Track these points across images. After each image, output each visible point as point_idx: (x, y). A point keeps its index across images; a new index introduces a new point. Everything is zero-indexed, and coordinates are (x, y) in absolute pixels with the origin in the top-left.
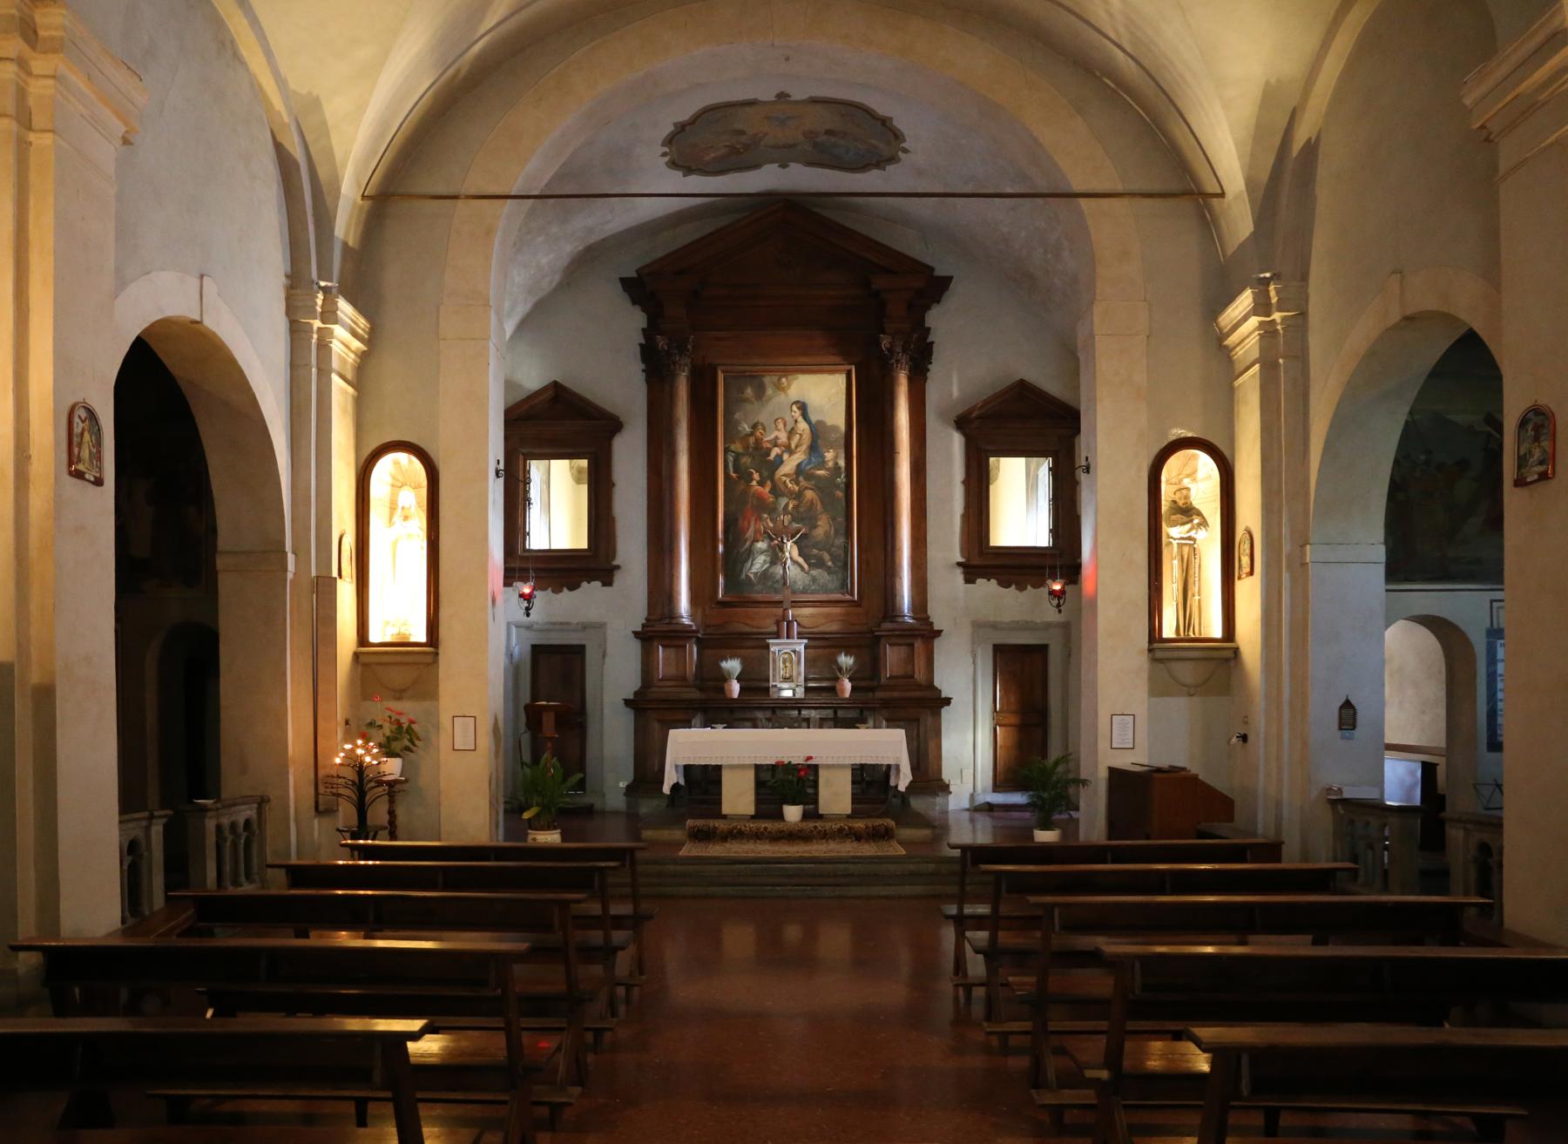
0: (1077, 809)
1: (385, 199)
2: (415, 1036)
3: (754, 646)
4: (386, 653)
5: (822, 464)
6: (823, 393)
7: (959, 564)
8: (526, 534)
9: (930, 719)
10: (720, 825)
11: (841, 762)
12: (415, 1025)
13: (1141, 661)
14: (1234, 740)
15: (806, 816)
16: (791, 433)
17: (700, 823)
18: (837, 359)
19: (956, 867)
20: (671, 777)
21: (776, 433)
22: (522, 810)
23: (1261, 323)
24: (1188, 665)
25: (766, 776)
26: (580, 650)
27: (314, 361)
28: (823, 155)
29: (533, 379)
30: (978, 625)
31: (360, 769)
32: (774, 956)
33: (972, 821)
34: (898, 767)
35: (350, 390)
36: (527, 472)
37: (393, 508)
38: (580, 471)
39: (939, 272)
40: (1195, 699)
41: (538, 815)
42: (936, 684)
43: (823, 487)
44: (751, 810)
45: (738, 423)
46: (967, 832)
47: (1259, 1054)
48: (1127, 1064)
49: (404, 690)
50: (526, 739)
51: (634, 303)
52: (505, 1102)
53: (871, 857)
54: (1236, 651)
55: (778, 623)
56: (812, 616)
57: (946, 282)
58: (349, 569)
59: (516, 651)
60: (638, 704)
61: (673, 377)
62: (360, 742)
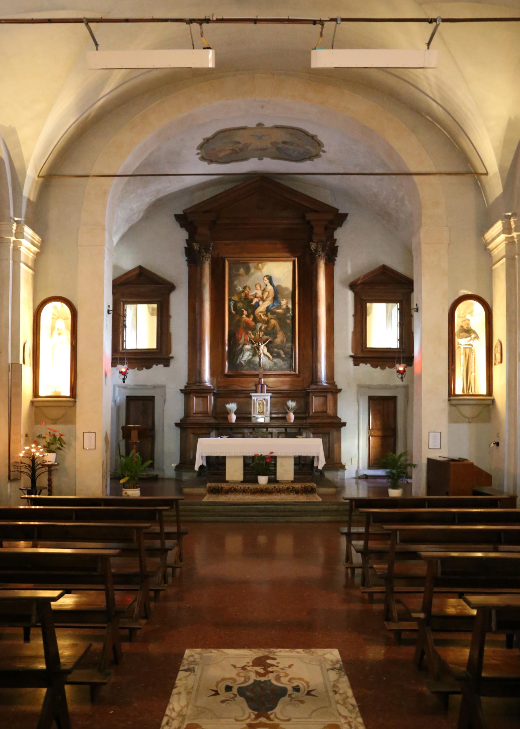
0: (411, 478)
1: (49, 178)
2: (55, 599)
3: (244, 397)
4: (48, 401)
5: (280, 307)
6: (281, 272)
7: (351, 356)
8: (123, 341)
9: (335, 434)
10: (225, 486)
11: (288, 455)
12: (55, 593)
13: (445, 405)
14: (492, 445)
15: (270, 481)
16: (264, 291)
17: (214, 485)
18: (288, 255)
19: (348, 507)
20: (199, 462)
21: (256, 291)
22: (120, 479)
23: (507, 238)
24: (467, 407)
25: (250, 461)
26: (151, 399)
27: (11, 257)
28: (281, 153)
29: (128, 264)
30: (360, 387)
31: (33, 459)
32: (252, 551)
33: (357, 483)
34: (318, 457)
35: (31, 271)
36: (124, 310)
37: (53, 329)
38: (153, 309)
39: (341, 211)
40: (472, 425)
41: (128, 481)
42: (339, 415)
43: (280, 318)
44: (241, 478)
45: (236, 286)
46: (356, 491)
47: (500, 610)
48: (434, 610)
49: (57, 420)
50: (123, 443)
51: (182, 227)
52: (105, 628)
53: (306, 502)
54: (493, 401)
55: (256, 386)
56: (275, 382)
57: (345, 216)
58: (29, 360)
59: (118, 399)
60: (183, 425)
61: (202, 264)
62: (33, 446)
